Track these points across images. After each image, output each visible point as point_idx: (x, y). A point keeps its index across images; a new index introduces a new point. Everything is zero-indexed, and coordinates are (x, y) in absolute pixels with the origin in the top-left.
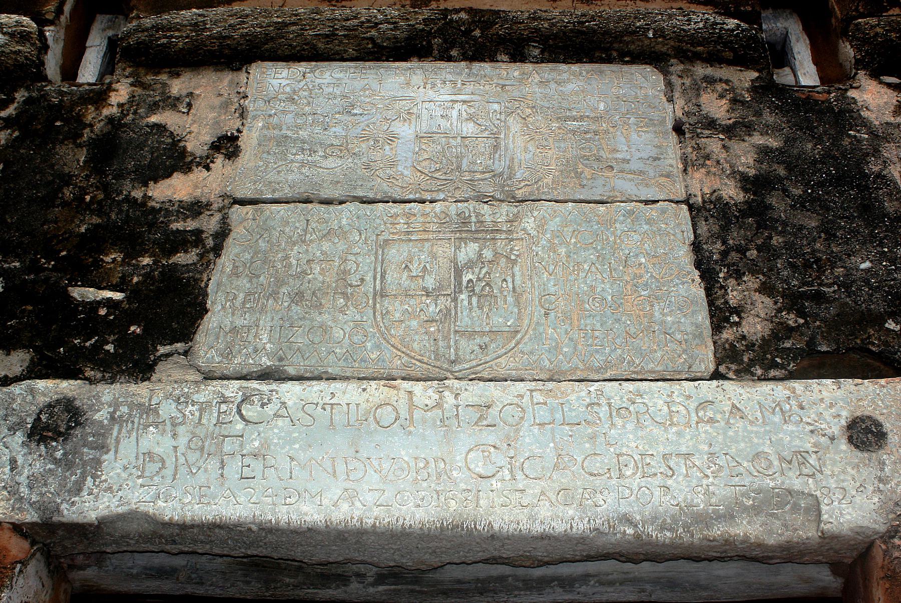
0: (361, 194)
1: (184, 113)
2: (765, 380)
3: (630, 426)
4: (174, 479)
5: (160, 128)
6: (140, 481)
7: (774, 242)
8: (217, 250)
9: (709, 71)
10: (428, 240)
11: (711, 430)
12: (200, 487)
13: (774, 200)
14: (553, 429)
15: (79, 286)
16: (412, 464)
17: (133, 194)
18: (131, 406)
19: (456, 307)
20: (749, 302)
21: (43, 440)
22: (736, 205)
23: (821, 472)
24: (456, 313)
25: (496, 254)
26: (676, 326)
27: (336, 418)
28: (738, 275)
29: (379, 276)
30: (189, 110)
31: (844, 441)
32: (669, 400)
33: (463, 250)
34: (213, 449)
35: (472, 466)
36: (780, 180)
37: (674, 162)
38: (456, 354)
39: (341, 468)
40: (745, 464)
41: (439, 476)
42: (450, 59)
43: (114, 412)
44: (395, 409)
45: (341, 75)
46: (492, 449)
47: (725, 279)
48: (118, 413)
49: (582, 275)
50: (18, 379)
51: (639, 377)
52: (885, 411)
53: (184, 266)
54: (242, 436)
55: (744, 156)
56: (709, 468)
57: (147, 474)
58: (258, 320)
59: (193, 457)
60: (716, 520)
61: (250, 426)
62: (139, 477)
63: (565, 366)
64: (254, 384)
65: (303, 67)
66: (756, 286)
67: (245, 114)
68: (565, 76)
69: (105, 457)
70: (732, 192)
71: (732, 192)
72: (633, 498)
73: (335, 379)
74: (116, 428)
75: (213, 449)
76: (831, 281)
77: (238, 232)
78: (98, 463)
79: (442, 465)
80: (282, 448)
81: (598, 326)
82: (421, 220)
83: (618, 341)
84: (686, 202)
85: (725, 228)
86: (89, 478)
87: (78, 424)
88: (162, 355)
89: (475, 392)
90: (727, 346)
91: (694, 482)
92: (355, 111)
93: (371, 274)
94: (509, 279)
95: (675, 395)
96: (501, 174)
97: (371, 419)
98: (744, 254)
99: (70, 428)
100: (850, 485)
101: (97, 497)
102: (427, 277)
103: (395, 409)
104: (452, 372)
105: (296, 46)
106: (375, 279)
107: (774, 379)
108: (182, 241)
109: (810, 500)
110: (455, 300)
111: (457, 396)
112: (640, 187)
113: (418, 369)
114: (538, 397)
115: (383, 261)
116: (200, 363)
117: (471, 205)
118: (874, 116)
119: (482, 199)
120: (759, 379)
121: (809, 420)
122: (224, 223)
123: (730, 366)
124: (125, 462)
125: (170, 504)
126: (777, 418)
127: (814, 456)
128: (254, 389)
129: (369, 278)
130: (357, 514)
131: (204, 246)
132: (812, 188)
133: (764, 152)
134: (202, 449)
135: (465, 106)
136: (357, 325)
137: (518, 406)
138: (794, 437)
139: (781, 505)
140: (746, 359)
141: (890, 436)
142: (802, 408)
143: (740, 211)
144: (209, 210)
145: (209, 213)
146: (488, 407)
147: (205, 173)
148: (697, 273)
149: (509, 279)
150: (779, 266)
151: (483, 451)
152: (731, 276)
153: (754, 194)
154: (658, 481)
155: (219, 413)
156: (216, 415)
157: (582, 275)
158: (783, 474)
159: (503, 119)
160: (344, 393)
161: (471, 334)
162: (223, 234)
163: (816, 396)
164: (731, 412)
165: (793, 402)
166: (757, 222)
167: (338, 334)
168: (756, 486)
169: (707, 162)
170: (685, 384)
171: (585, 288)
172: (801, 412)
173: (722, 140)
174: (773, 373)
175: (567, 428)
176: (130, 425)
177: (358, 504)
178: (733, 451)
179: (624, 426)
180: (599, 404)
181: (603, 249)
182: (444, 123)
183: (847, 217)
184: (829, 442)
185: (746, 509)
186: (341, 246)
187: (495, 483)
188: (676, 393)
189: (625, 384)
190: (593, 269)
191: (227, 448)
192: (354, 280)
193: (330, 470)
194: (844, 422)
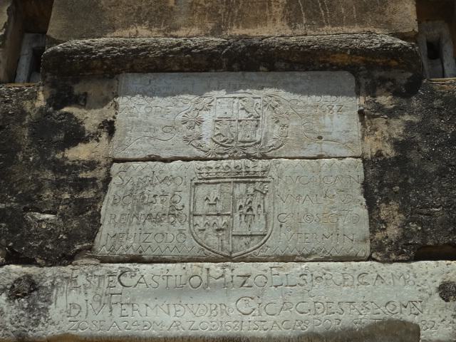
0: (183, 156)
5: (70, 115)
7: (409, 181)
8: (105, 189)
9: (383, 73)
10: (219, 183)
13: (412, 155)
17: (57, 156)
22: (390, 159)
23: (422, 312)
25: (255, 190)
28: (387, 201)
29: (192, 204)
30: (86, 103)
31: (437, 295)
36: (416, 143)
37: (356, 133)
38: (232, 247)
41: (222, 313)
42: (232, 70)
43: (54, 281)
45: (171, 81)
46: (250, 300)
47: (380, 203)
54: (121, 294)
55: (397, 128)
56: (362, 309)
62: (68, 317)
64: (127, 265)
65: (150, 76)
66: (396, 208)
68: (298, 79)
69: (50, 306)
70: (389, 151)
71: (389, 151)
74: (55, 291)
75: (106, 302)
76: (439, 204)
77: (116, 180)
78: (47, 309)
79: (224, 307)
82: (216, 171)
87: (36, 289)
92: (179, 105)
93: (188, 203)
94: (262, 205)
96: (259, 143)
97: (188, 284)
101: (47, 328)
106: (190, 205)
108: (82, 185)
110: (232, 217)
115: (194, 196)
123: (378, 253)
124: (60, 309)
126: (401, 282)
128: (127, 268)
132: (436, 147)
133: (409, 125)
134: (100, 301)
135: (241, 100)
136: (181, 231)
138: (410, 293)
140: (387, 249)
142: (416, 277)
146: (249, 276)
153: (401, 153)
158: (401, 313)
162: (108, 180)
165: (411, 274)
169: (376, 133)
184: (428, 296)
186: (172, 186)
192: (179, 206)
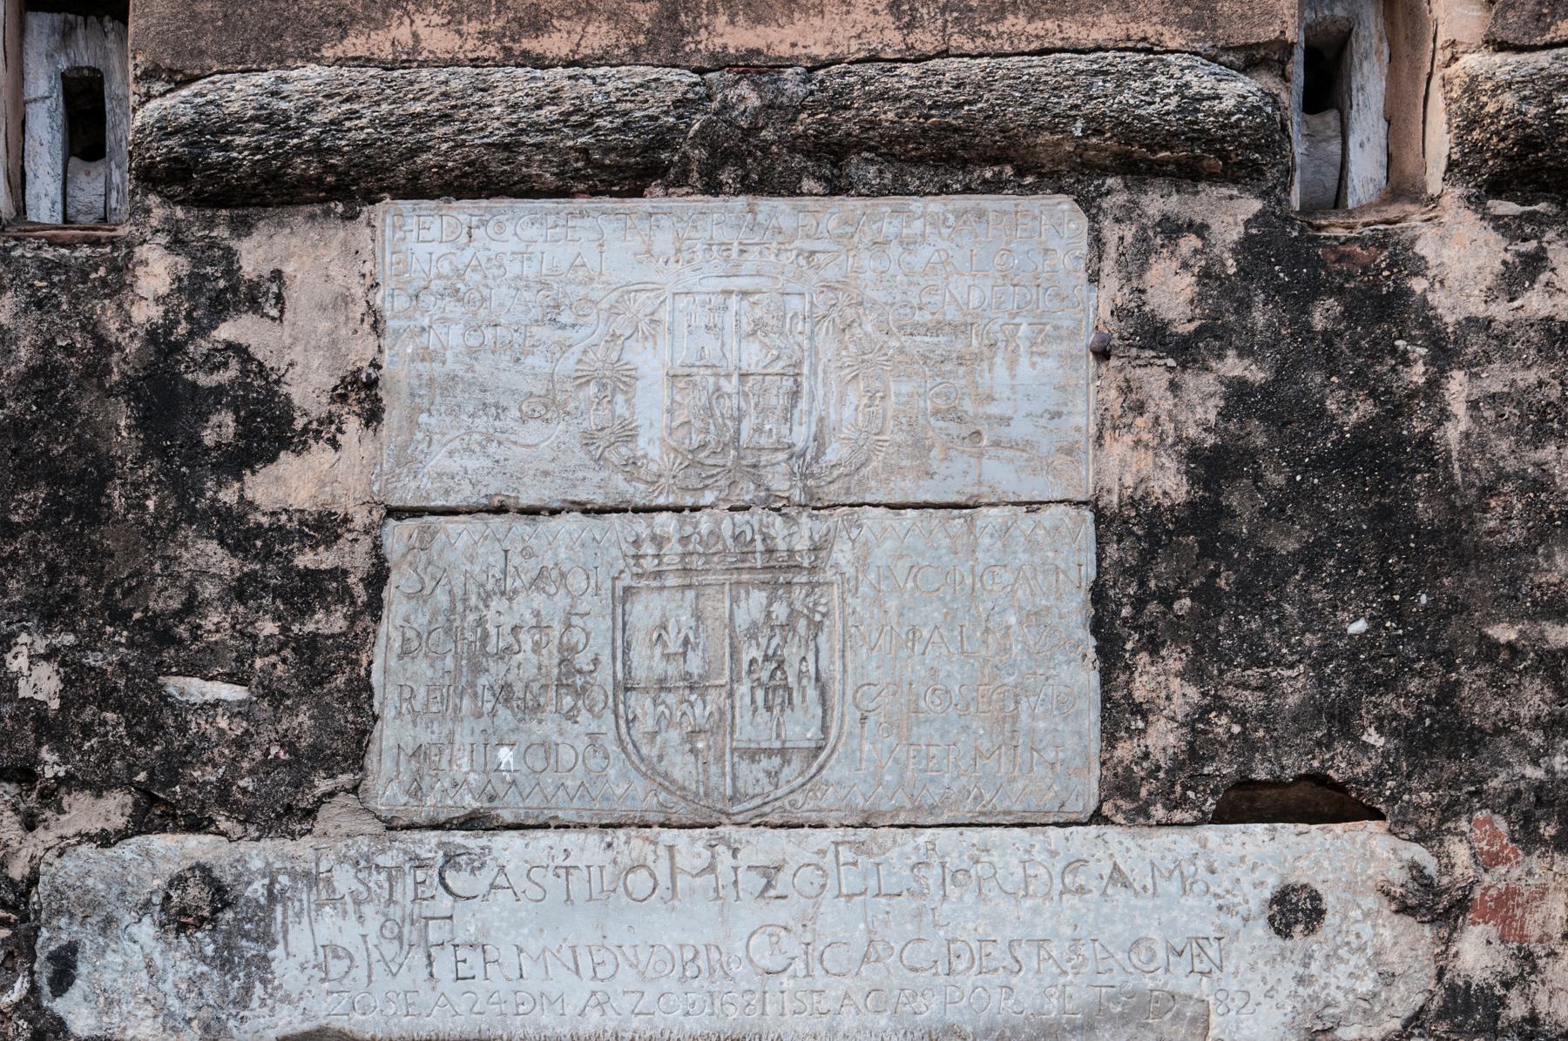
0: (583, 497)
1: (273, 319)
2: (1166, 825)
3: (970, 898)
4: (370, 981)
6: (326, 985)
8: (375, 607)
11: (1079, 905)
12: (406, 993)
14: (864, 903)
15: (177, 674)
16: (677, 955)
18: (293, 875)
19: (733, 707)
20: (1163, 695)
21: (182, 928)
22: (1172, 509)
23: (1221, 969)
24: (733, 717)
26: (1049, 737)
27: (573, 888)
28: (1153, 646)
29: (619, 655)
31: (1263, 921)
32: (1026, 857)
33: (743, 604)
34: (415, 938)
35: (756, 958)
38: (734, 785)
39: (585, 963)
40: (1119, 956)
41: (712, 971)
43: (272, 883)
44: (652, 875)
46: (783, 933)
47: (1134, 652)
48: (278, 887)
49: (918, 648)
50: (123, 835)
51: (988, 821)
52: (1331, 876)
53: (328, 637)
57: (333, 975)
58: (452, 733)
59: (390, 949)
60: (1070, 1032)
61: (461, 904)
62: (323, 980)
63: (885, 806)
64: (458, 837)
67: (381, 326)
72: (964, 1002)
73: (567, 827)
74: (279, 909)
78: (264, 961)
79: (715, 955)
80: (506, 934)
81: (936, 739)
83: (963, 764)
84: (1093, 504)
85: (1147, 558)
86: (257, 984)
88: (324, 795)
89: (764, 846)
90: (1120, 770)
91: (1048, 981)
93: (607, 651)
95: (1034, 851)
97: (621, 890)
98: (1170, 606)
99: (215, 911)
100: (1257, 992)
101: (272, 1009)
102: (690, 654)
103: (652, 875)
104: (728, 815)
105: (452, 170)
106: (614, 658)
107: (1181, 824)
109: (1199, 1008)
110: (731, 694)
111: (735, 852)
112: (1023, 476)
113: (682, 812)
114: (846, 854)
116: (380, 805)
117: (757, 516)
118: (1448, 302)
119: (774, 505)
120: (1159, 824)
121: (1219, 891)
122: (378, 556)
125: (369, 1017)
126: (1174, 887)
127: (1215, 944)
129: (605, 658)
130: (610, 1026)
131: (353, 603)
134: (400, 938)
137: (818, 867)
138: (1193, 915)
139: (1160, 1014)
141: (1328, 917)
143: (1178, 520)
144: (349, 531)
145: (350, 536)
146: (778, 869)
147: (330, 455)
148: (1092, 642)
149: (811, 658)
150: (1221, 628)
151: (771, 935)
152: (1143, 648)
154: (999, 978)
155: (416, 883)
156: (412, 886)
157: (918, 648)
159: (807, 331)
160: (582, 850)
161: (753, 755)
162: (378, 578)
163: (1235, 851)
164: (1111, 877)
165: (1201, 863)
166: (1202, 544)
167: (567, 755)
168: (1130, 986)
170: (1052, 831)
171: (923, 673)
172: (1210, 877)
173: (1171, 369)
174: (1178, 816)
175: (883, 900)
176: (297, 904)
177: (610, 1012)
178: (1104, 938)
179: (961, 898)
180: (927, 864)
181: (954, 599)
182: (711, 346)
183: (1350, 532)
185: (1112, 1018)
186: (562, 601)
187: (786, 981)
188: (1038, 847)
189: (967, 831)
190: (936, 638)
191: (433, 937)
193: (572, 965)
194: (1267, 894)
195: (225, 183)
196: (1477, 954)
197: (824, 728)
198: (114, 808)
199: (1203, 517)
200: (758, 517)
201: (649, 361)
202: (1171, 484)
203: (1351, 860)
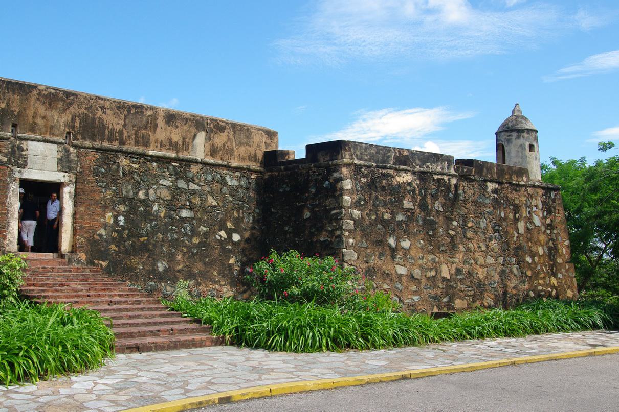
195: (21, 139)
196: (71, 179)
197: (90, 381)
198: (16, 167)
199: (61, 159)
200: (44, 157)
201: (39, 149)
202: (60, 158)
203: (66, 174)
